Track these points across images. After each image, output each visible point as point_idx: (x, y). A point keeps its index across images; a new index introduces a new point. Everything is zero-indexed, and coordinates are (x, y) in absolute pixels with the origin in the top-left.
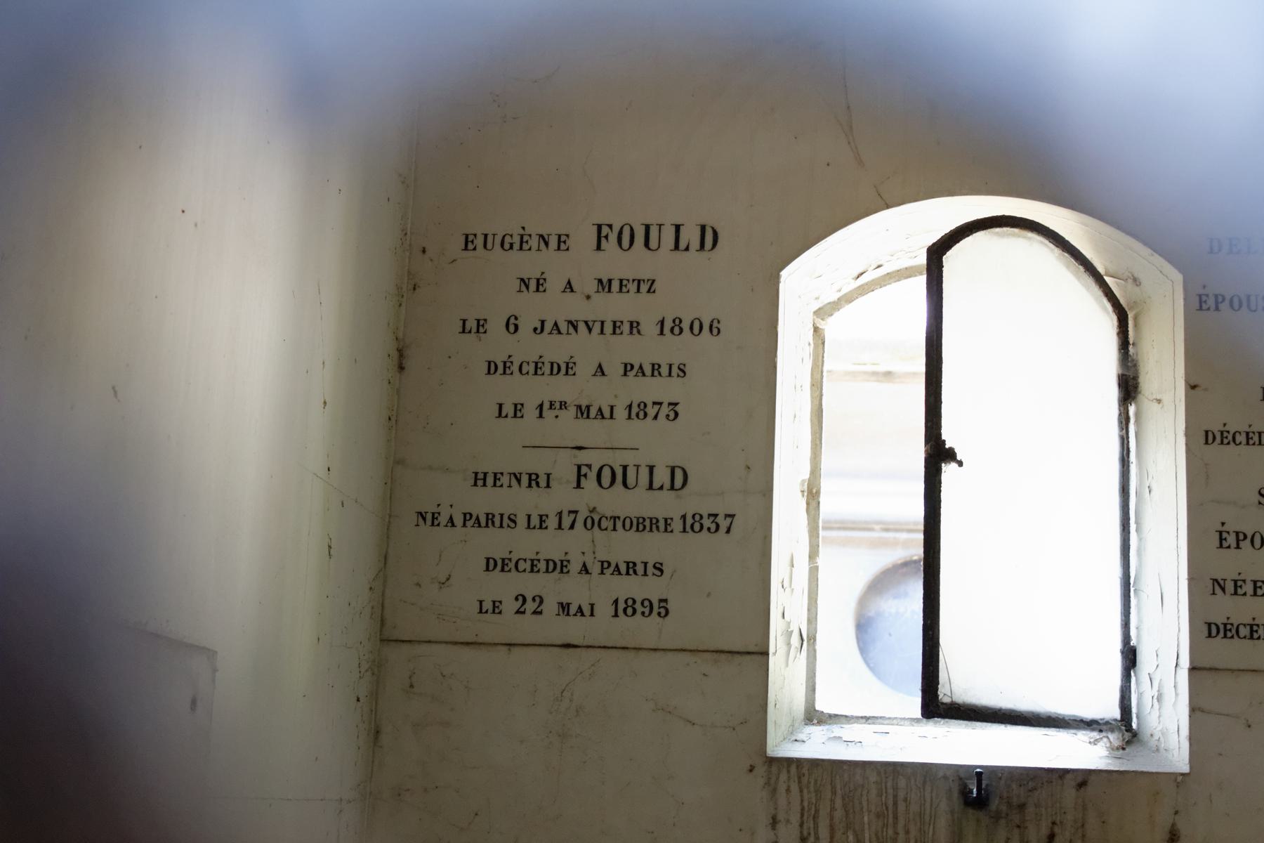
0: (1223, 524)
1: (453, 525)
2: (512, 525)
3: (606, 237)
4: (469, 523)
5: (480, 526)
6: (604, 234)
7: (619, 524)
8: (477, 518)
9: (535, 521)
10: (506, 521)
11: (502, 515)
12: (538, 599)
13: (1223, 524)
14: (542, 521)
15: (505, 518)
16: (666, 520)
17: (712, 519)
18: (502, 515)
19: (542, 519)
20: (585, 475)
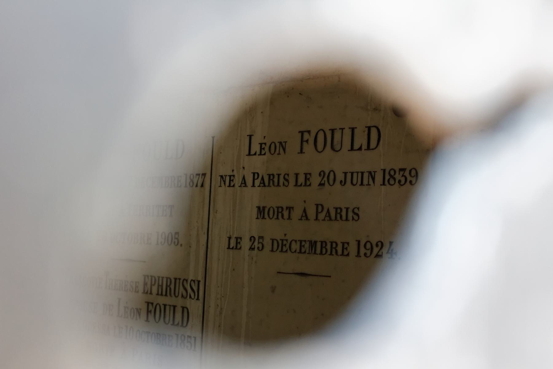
0: (285, 235)
1: (307, 219)
2: (356, 217)
3: (307, 141)
4: (322, 216)
5: (330, 219)
6: (305, 138)
7: (339, 249)
8: (263, 178)
9: (301, 179)
10: (350, 214)
11: (347, 209)
12: (380, 244)
13: (285, 235)
14: (306, 179)
15: (282, 178)
16: (343, 244)
17: (402, 173)
18: (347, 209)
19: (307, 176)
20: (307, 141)
